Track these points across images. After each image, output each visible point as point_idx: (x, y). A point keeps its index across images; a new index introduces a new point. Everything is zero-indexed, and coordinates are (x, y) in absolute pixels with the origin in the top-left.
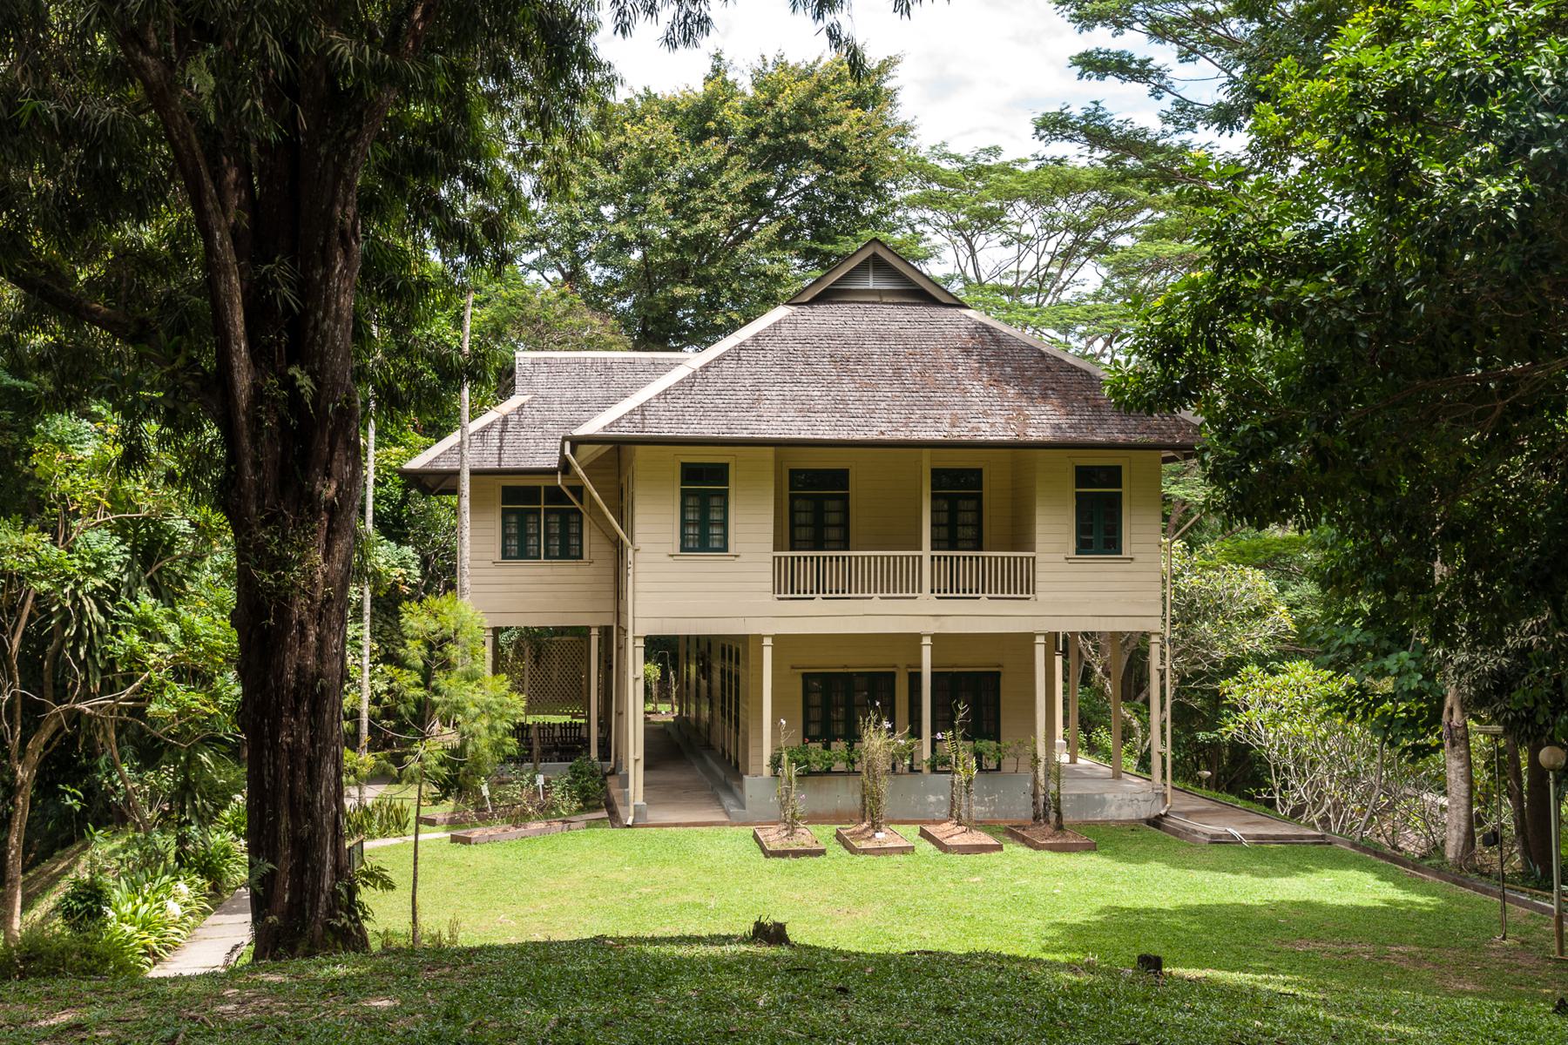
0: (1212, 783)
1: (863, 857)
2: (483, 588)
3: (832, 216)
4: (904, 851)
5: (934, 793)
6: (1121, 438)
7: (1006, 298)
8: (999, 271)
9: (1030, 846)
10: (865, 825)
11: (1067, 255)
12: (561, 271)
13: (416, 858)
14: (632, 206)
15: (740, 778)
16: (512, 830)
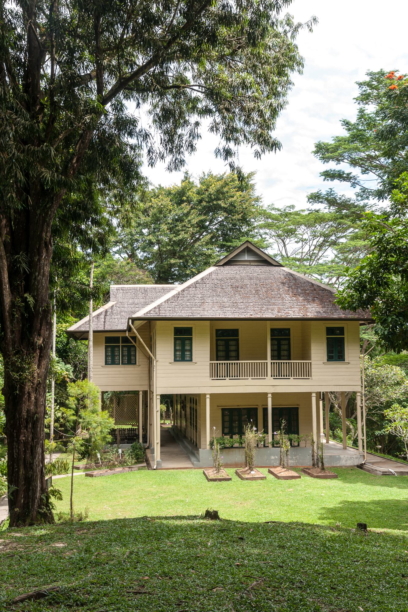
0: (382, 450)
1: (246, 481)
2: (97, 376)
3: (230, 232)
4: (262, 478)
5: (273, 455)
6: (343, 316)
7: (297, 263)
8: (295, 252)
9: (312, 477)
10: (247, 468)
11: (321, 246)
12: (128, 254)
13: (72, 483)
14: (154, 229)
15: (198, 450)
16: (109, 471)
